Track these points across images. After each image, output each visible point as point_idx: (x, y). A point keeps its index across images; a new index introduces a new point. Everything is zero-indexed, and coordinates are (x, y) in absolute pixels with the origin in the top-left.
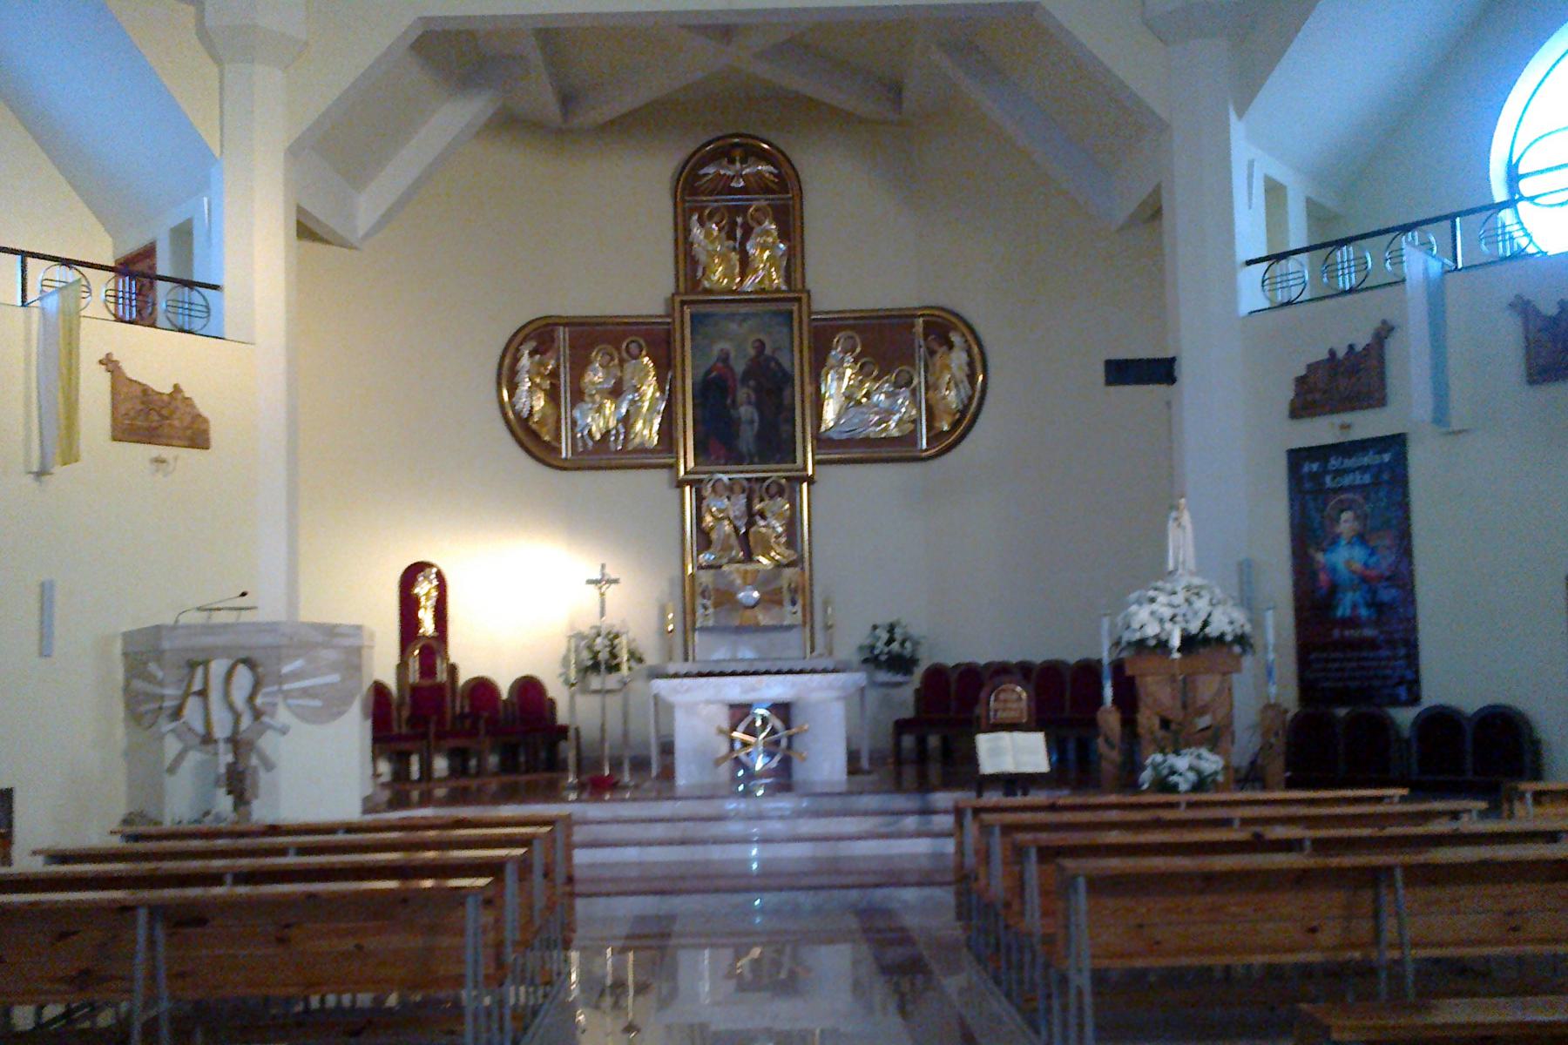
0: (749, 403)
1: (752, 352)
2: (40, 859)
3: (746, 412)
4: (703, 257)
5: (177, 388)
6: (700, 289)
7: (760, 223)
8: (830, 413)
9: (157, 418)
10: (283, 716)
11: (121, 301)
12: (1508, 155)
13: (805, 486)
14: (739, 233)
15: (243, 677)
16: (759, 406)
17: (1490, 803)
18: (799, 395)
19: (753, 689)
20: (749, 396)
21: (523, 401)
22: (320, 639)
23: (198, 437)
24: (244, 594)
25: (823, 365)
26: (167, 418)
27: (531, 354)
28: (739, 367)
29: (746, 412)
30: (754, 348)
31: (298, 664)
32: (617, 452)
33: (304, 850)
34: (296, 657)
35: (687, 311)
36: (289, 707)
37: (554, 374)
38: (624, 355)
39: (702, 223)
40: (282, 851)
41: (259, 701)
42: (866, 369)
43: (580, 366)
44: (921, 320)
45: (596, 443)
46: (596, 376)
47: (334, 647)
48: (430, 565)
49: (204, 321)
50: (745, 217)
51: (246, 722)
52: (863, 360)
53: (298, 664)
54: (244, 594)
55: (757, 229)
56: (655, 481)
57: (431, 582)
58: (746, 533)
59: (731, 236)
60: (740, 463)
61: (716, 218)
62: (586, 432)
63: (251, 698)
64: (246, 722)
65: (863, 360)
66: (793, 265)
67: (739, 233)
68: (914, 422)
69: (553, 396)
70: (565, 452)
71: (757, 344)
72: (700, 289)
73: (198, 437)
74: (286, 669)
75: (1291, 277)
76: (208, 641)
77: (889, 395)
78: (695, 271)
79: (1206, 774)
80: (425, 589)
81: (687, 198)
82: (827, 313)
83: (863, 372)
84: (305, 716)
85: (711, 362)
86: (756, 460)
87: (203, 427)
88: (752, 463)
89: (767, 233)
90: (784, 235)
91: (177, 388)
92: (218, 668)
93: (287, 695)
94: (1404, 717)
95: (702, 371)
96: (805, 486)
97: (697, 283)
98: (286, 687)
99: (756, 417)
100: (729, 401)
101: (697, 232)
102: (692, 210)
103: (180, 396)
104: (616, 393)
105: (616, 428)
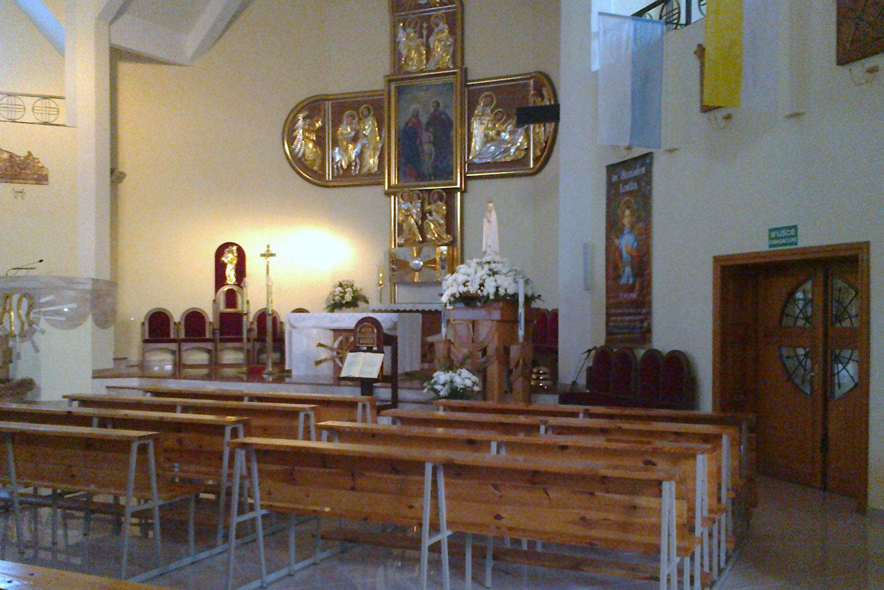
0: (430, 142)
1: (432, 109)
2: (76, 403)
3: (428, 148)
4: (404, 52)
5: (30, 154)
6: (402, 72)
7: (437, 25)
8: (477, 144)
9: (18, 170)
10: (43, 324)
11: (13, 110)
12: (228, 33)
13: (459, 193)
14: (425, 32)
15: (25, 302)
16: (434, 144)
17: (164, 368)
18: (457, 133)
19: (336, 320)
20: (429, 137)
21: (298, 145)
22: (64, 285)
23: (41, 179)
24: (41, 261)
25: (473, 116)
26: (24, 169)
27: (304, 118)
28: (424, 119)
29: (428, 148)
30: (433, 106)
31: (50, 298)
32: (356, 175)
33: (186, 409)
34: (48, 294)
35: (393, 86)
36: (47, 320)
37: (322, 128)
38: (361, 115)
39: (404, 28)
40: (172, 408)
41: (32, 316)
42: (498, 117)
43: (337, 123)
44: (330, 102)
45: (345, 170)
46: (346, 130)
47: (73, 289)
48: (233, 244)
49: (56, 116)
50: (428, 22)
51: (26, 327)
52: (496, 111)
53: (50, 298)
54: (41, 261)
55: (436, 30)
56: (374, 193)
57: (233, 253)
58: (422, 224)
59: (421, 36)
60: (423, 180)
61: (412, 26)
62: (339, 165)
63: (28, 314)
64: (26, 327)
65: (496, 111)
66: (458, 51)
67: (425, 32)
68: (526, 149)
69: (320, 143)
70: (329, 176)
71: (435, 104)
72: (402, 72)
73: (41, 179)
74: (43, 300)
75: (40, 112)
76: (12, 285)
77: (512, 133)
78: (400, 60)
79: (220, 362)
80: (230, 258)
81: (396, 14)
82: (507, 77)
83: (496, 119)
84: (55, 324)
85: (408, 118)
86: (433, 178)
87: (44, 173)
88: (430, 180)
89: (442, 31)
90: (452, 32)
91: (30, 154)
92: (15, 298)
93: (45, 313)
94: (640, 353)
95: (402, 125)
96: (459, 193)
97: (401, 67)
98: (43, 309)
99: (433, 149)
100: (418, 142)
101: (402, 37)
102: (399, 21)
103: (31, 158)
104: (355, 140)
105: (355, 161)
